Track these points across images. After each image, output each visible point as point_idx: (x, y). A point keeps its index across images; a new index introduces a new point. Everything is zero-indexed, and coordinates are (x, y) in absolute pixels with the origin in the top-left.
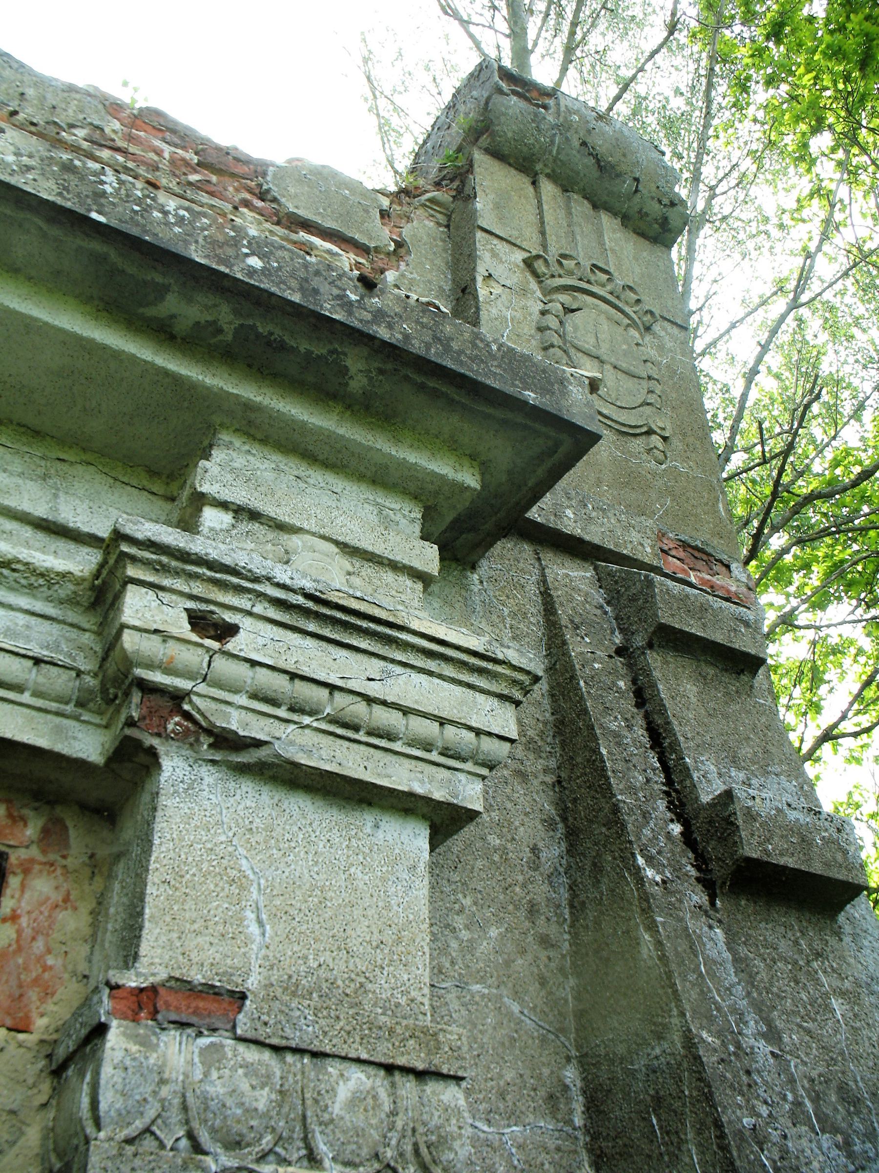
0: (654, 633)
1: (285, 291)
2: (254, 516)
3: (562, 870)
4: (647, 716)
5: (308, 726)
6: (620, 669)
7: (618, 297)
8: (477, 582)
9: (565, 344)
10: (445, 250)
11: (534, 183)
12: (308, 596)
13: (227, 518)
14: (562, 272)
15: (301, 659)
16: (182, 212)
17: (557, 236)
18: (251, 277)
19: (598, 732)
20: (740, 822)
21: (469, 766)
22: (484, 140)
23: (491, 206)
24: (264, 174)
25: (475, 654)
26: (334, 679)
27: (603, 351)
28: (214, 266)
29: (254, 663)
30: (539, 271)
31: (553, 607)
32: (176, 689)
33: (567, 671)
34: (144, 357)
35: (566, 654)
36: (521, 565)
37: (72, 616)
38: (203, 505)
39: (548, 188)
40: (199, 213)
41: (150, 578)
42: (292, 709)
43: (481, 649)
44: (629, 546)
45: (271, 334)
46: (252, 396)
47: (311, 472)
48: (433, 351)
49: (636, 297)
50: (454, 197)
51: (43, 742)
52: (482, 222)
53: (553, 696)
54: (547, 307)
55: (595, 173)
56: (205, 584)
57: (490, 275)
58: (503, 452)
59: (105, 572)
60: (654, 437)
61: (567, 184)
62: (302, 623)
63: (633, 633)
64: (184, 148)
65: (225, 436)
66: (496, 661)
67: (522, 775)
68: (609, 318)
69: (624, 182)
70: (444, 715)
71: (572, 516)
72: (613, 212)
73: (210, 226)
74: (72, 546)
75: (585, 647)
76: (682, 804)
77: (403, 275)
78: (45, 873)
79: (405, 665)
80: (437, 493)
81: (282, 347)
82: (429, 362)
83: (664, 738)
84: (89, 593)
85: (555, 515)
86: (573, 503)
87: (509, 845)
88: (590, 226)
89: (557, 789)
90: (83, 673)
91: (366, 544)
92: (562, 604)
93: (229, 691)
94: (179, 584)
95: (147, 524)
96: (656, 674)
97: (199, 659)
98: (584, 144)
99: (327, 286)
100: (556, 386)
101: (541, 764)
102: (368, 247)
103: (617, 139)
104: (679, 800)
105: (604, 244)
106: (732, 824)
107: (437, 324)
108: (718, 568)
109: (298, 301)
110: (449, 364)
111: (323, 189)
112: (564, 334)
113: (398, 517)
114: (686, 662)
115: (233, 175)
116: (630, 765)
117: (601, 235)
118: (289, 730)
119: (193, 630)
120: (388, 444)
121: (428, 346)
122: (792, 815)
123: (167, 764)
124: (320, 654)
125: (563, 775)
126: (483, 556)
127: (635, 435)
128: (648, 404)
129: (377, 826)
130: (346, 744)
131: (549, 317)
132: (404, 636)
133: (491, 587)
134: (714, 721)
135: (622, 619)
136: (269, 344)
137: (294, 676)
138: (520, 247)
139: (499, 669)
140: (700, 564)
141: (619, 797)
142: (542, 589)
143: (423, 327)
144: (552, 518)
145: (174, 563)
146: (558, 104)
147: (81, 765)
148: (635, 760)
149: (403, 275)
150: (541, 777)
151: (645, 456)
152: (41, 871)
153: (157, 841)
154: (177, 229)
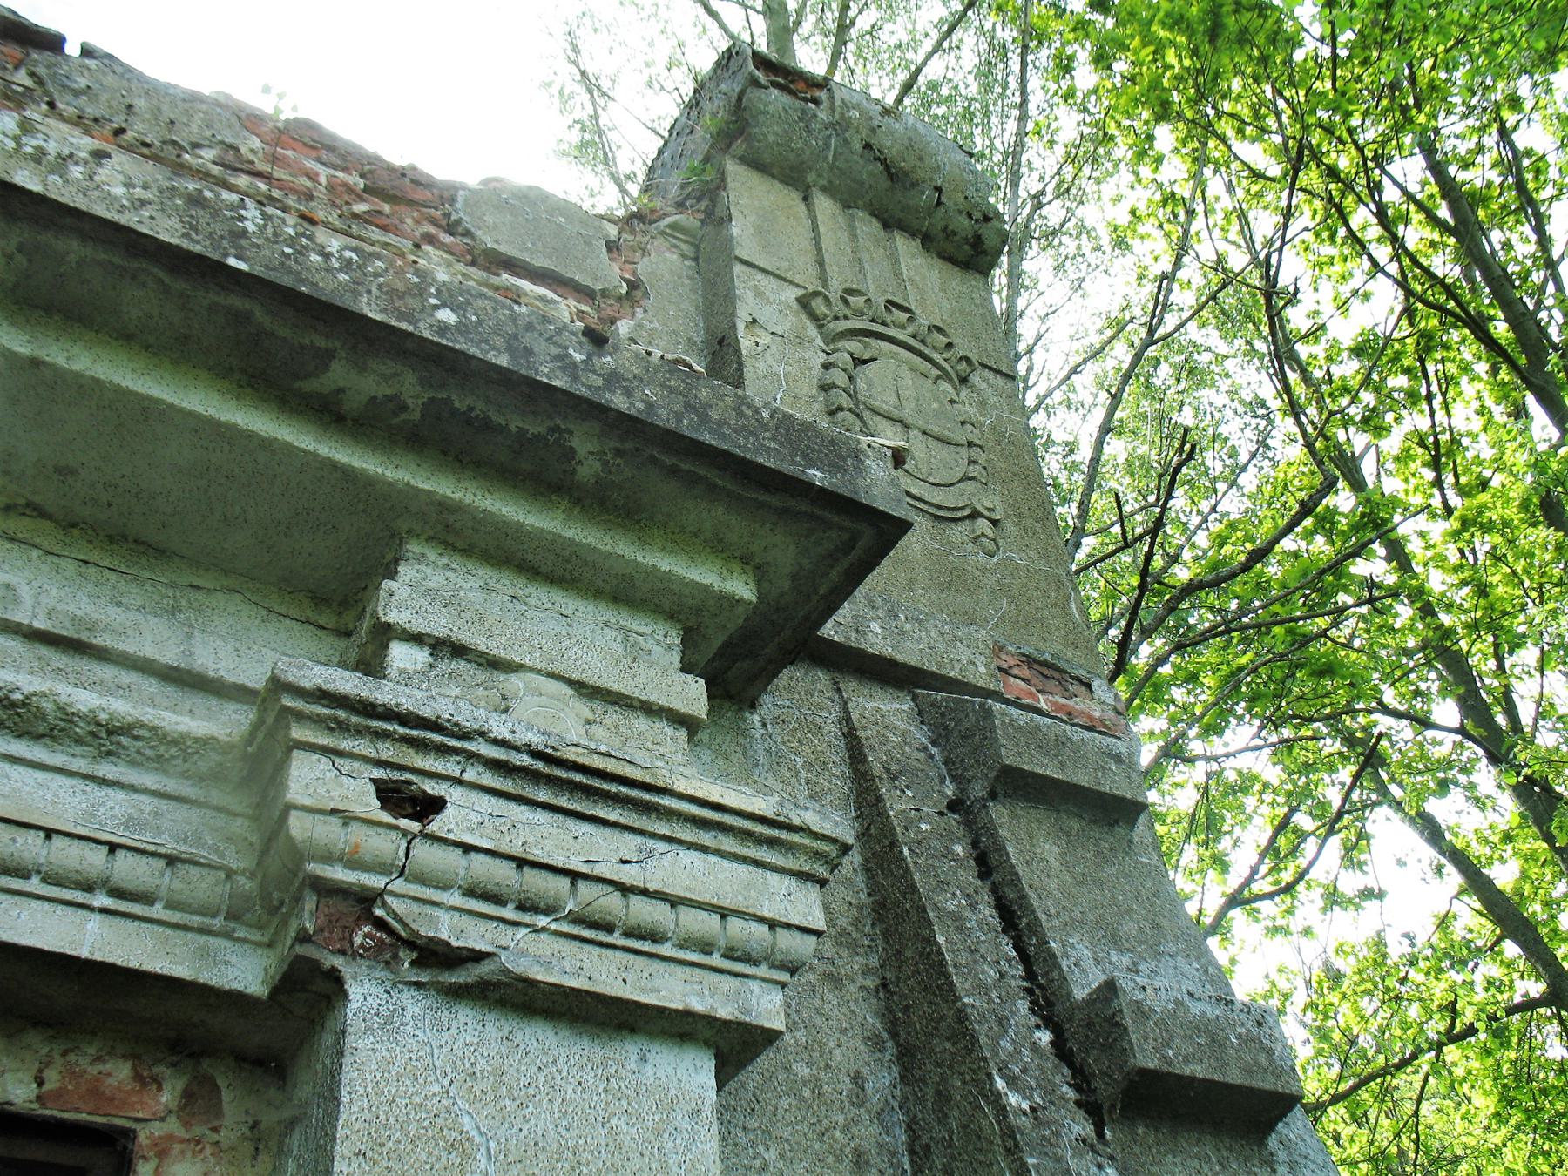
0: (997, 778)
2: (459, 651)
3: (895, 1104)
5: (543, 929)
7: (923, 342)
8: (758, 725)
9: (857, 405)
11: (805, 199)
12: (537, 755)
13: (422, 656)
14: (848, 312)
15: (531, 839)
16: (348, 254)
18: (442, 336)
20: (1128, 1023)
21: (763, 970)
22: (739, 146)
24: (452, 201)
25: (762, 820)
26: (575, 864)
27: (907, 413)
29: (467, 848)
30: (819, 312)
31: (861, 753)
32: (364, 888)
34: (303, 446)
35: (883, 813)
36: (816, 699)
38: (389, 640)
41: (324, 740)
42: (521, 907)
43: (769, 814)
45: (471, 409)
47: (531, 589)
49: (946, 340)
50: (702, 221)
51: (182, 971)
52: (739, 252)
54: (832, 358)
55: (884, 183)
57: (755, 320)
58: (783, 550)
60: (980, 521)
64: (345, 170)
65: (414, 547)
66: (790, 828)
67: (834, 980)
70: (726, 903)
73: (386, 270)
74: (213, 702)
77: (640, 325)
78: (189, 1154)
79: (669, 840)
80: (699, 610)
81: (487, 426)
83: (1020, 918)
86: (880, 613)
87: (822, 1075)
91: (610, 682)
92: (872, 748)
93: (436, 887)
94: (363, 747)
95: (316, 669)
97: (394, 847)
98: (868, 146)
99: (544, 344)
100: (849, 461)
101: (858, 963)
103: (910, 139)
104: (1046, 999)
106: (1118, 1024)
107: (689, 388)
115: (411, 203)
116: (978, 956)
121: (679, 417)
122: (1196, 1008)
123: (354, 990)
124: (555, 831)
125: (888, 975)
128: (971, 478)
129: (644, 1060)
130: (597, 950)
131: (833, 371)
132: (666, 801)
134: (1084, 890)
136: (468, 422)
137: (521, 863)
138: (791, 283)
140: (1051, 685)
141: (966, 1000)
144: (853, 635)
145: (354, 719)
146: (832, 98)
147: (235, 1000)
148: (982, 949)
149: (640, 325)
150: (860, 980)
151: (970, 547)
152: (182, 1152)
153: (345, 1099)
154: (342, 277)
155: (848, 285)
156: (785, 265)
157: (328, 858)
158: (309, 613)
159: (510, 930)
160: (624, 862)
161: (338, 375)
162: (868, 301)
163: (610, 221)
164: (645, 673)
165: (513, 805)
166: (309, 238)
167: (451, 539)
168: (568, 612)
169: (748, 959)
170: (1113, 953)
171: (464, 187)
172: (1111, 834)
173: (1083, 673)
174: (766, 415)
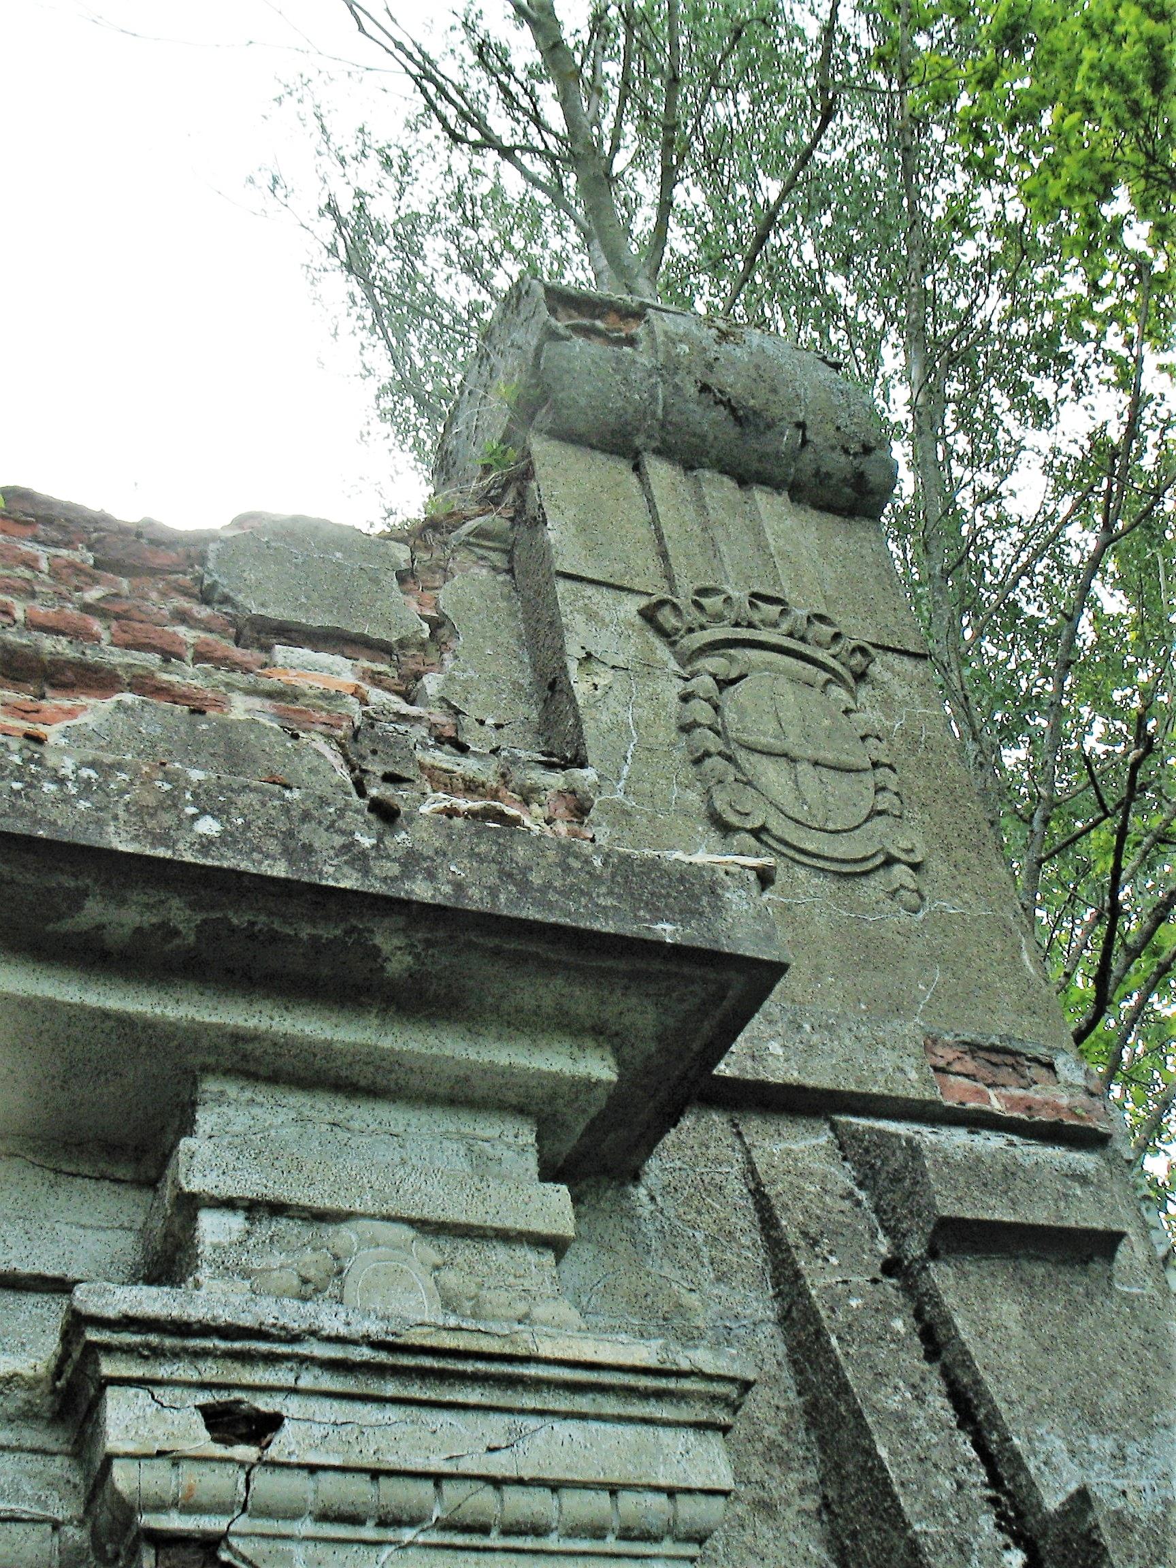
0: (934, 1232)
1: (260, 863)
2: (277, 1209)
4: (946, 1373)
5: (411, 1544)
6: (893, 1300)
7: (803, 639)
8: (645, 1200)
9: (727, 744)
10: (513, 614)
11: (637, 468)
13: (237, 1222)
14: (703, 620)
16: (86, 773)
17: (687, 556)
18: (206, 856)
19: (869, 1420)
20: (1107, 1540)
21: (667, 1547)
22: (544, 417)
23: (573, 530)
24: (202, 560)
26: (437, 1464)
27: (791, 743)
28: (148, 853)
29: (313, 1469)
30: (668, 626)
31: (772, 1216)
32: (205, 1533)
33: (808, 1321)
34: (67, 999)
35: (804, 1293)
36: (712, 1152)
37: (32, 1437)
38: (198, 1209)
39: (660, 472)
40: (111, 766)
41: (136, 1370)
42: (382, 1523)
43: (653, 1362)
44: (881, 1078)
45: (252, 924)
46: (241, 1022)
47: (352, 1110)
48: (502, 897)
49: (831, 631)
50: (512, 520)
53: (795, 1362)
55: (733, 431)
56: (220, 1362)
57: (589, 655)
58: (643, 1016)
59: (68, 1371)
61: (689, 457)
62: (375, 1387)
63: (904, 1235)
64: (68, 545)
65: (211, 1086)
66: (680, 1374)
67: (765, 1507)
68: (794, 680)
69: (782, 434)
70: (614, 1477)
71: (780, 1051)
72: (774, 484)
73: (131, 783)
75: (832, 1274)
76: (1020, 1515)
77: (451, 679)
79: (541, 1413)
80: (553, 1097)
81: (274, 938)
82: (499, 918)
83: (977, 1407)
84: (50, 1398)
85: (753, 1057)
86: (780, 1027)
88: (739, 520)
89: (825, 1518)
90: (63, 1523)
91: (454, 1215)
92: (785, 1207)
93: (285, 1518)
94: (182, 1371)
95: (118, 1292)
96: (950, 1300)
97: (231, 1482)
98: (705, 388)
101: (793, 1481)
102: (388, 644)
103: (757, 367)
104: (1015, 1508)
105: (767, 546)
106: (1096, 1544)
108: (1035, 1072)
109: (283, 875)
110: (531, 913)
111: (300, 560)
112: (724, 728)
113: (500, 1150)
114: (996, 1264)
115: (153, 572)
116: (929, 1465)
117: (759, 532)
118: (383, 1557)
119: (215, 1440)
120: (463, 1044)
121: (493, 892)
124: (410, 1428)
125: (831, 1494)
126: (649, 1154)
127: (866, 874)
128: (880, 813)
130: (473, 1556)
131: (694, 703)
132: (532, 1371)
133: (670, 1202)
134: (1054, 1358)
135: (885, 1212)
136: (252, 937)
137: (375, 1474)
138: (630, 591)
139: (687, 1385)
140: (1004, 1074)
141: (917, 1527)
142: (752, 1186)
143: (481, 861)
144: (749, 1063)
145: (169, 1342)
146: (651, 332)
148: (935, 1455)
149: (451, 679)
150: (798, 1503)
151: (888, 905)
154: (83, 805)
155: (699, 584)
156: (619, 567)
157: (160, 1507)
158: (102, 1165)
159: (373, 1551)
160: (491, 1450)
161: (94, 911)
162: (728, 600)
163: (397, 540)
164: (496, 1191)
165: (358, 1407)
166: (40, 763)
167: (252, 1067)
168: (399, 1130)
169: (647, 1537)
170: (1093, 1438)
171: (212, 537)
172: (1085, 1272)
173: (1041, 1052)
174: (598, 862)
